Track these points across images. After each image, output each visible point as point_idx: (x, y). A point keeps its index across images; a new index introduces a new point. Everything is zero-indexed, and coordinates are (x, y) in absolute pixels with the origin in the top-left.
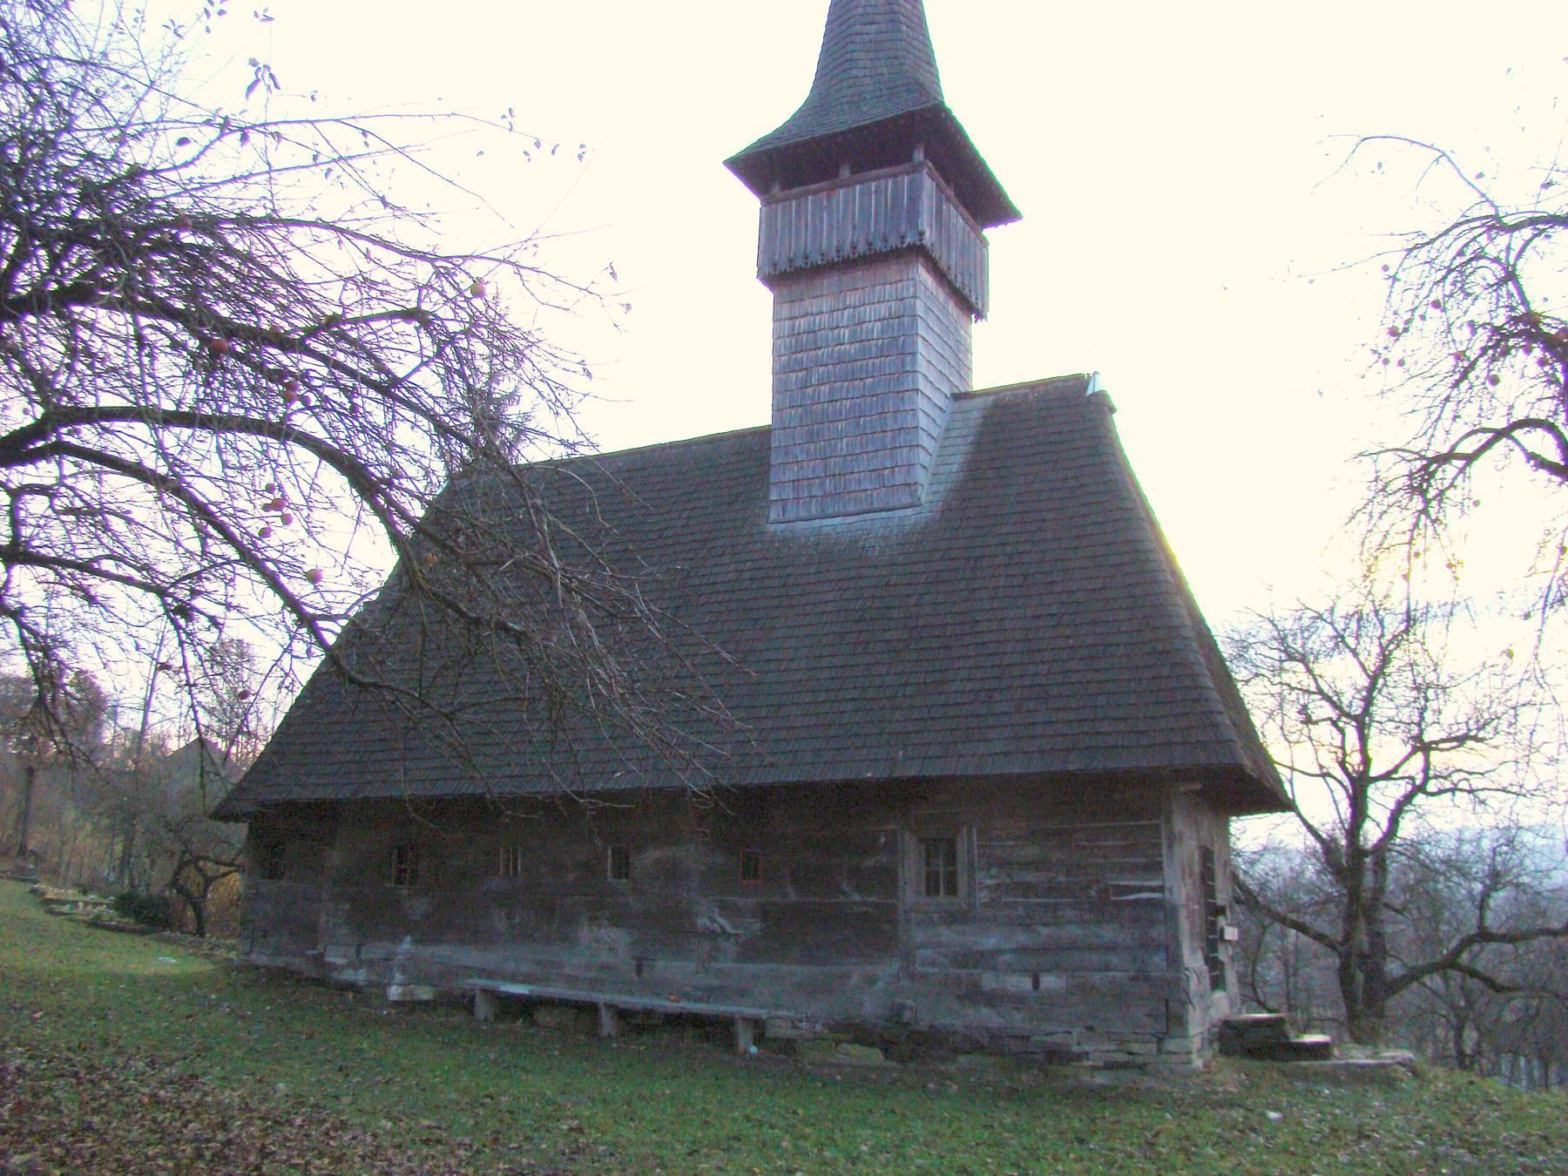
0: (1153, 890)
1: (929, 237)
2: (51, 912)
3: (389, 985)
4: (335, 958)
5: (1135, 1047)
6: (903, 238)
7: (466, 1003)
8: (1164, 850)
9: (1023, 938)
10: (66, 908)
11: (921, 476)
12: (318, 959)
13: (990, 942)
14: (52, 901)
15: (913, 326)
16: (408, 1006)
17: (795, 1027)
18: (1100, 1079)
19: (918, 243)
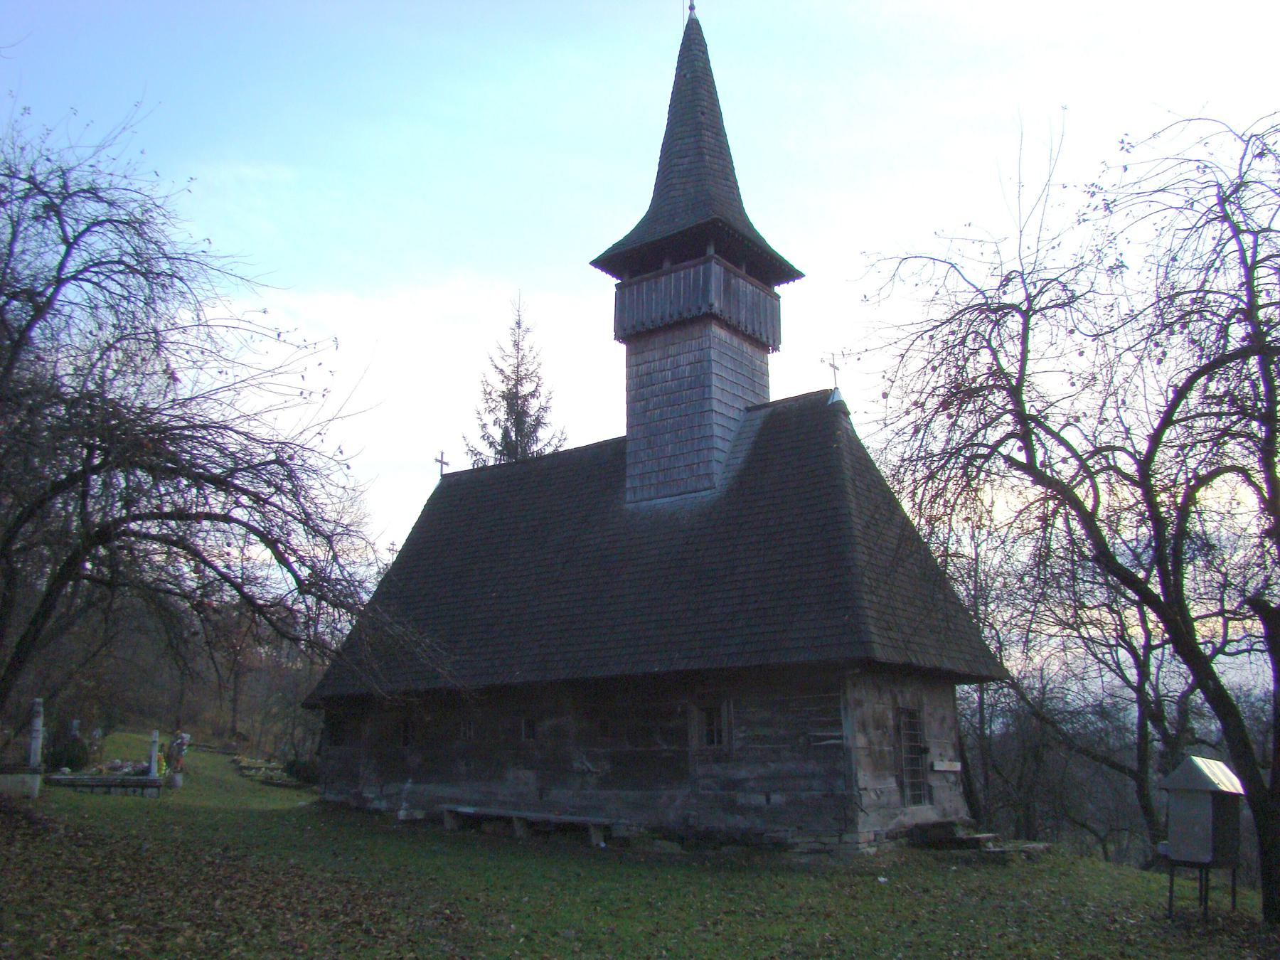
0: (836, 738)
1: (717, 305)
2: (243, 776)
3: (399, 810)
4: (368, 794)
5: (826, 840)
6: (700, 309)
7: (435, 820)
8: (843, 713)
9: (761, 771)
10: (253, 772)
11: (716, 468)
12: (358, 795)
13: (743, 774)
14: (245, 768)
15: (710, 367)
16: (412, 822)
17: (628, 830)
18: (804, 860)
19: (709, 311)
